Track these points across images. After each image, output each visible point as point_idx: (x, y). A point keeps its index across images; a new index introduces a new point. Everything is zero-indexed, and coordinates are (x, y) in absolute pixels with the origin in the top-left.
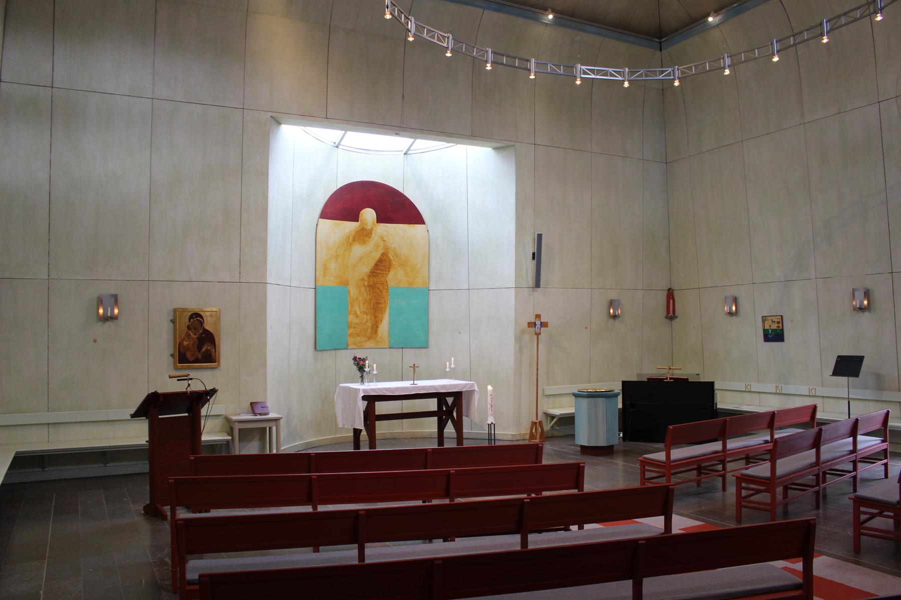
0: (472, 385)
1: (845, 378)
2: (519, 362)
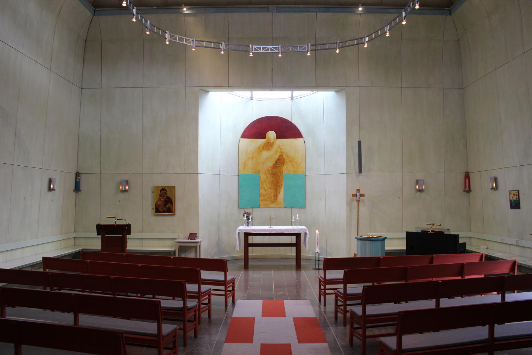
0: (305, 230)
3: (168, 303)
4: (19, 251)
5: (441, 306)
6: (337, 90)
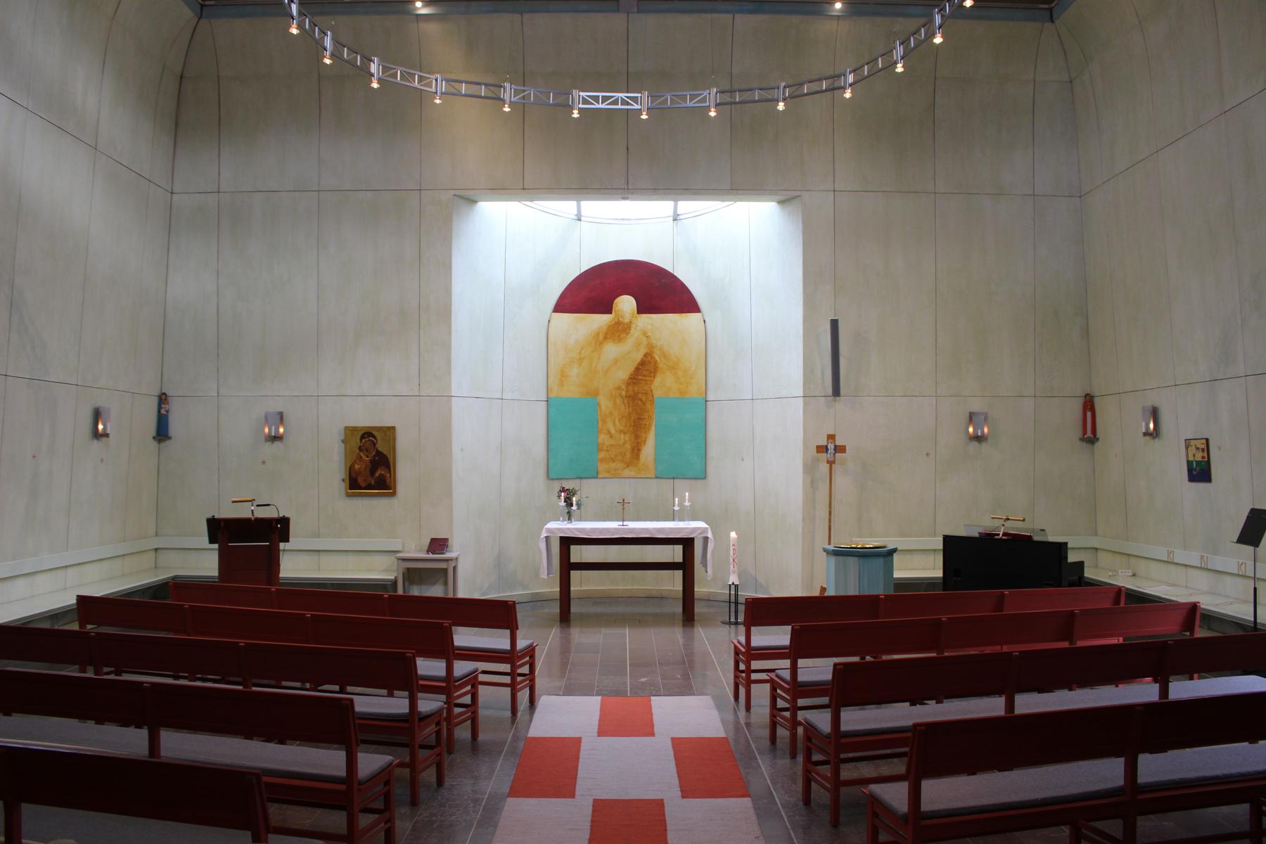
0: (705, 530)
2: (810, 502)
3: (372, 702)
4: (21, 583)
5: (1019, 710)
6: (782, 198)
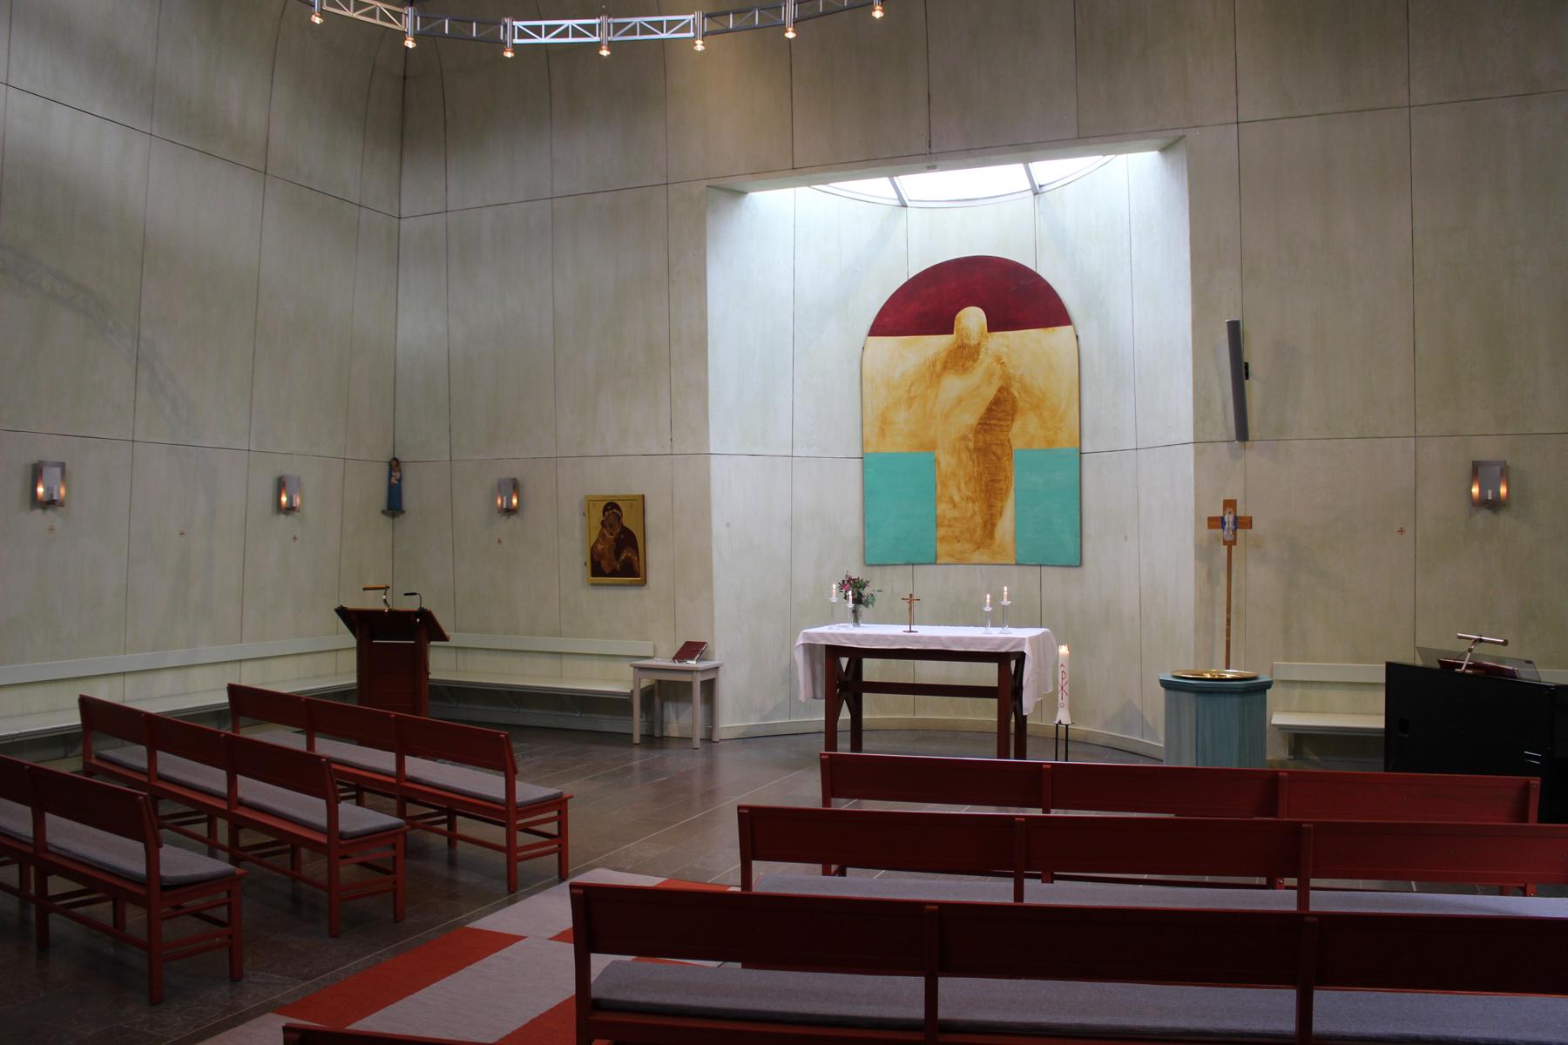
1: (1383, 680)
4: (168, 677)
